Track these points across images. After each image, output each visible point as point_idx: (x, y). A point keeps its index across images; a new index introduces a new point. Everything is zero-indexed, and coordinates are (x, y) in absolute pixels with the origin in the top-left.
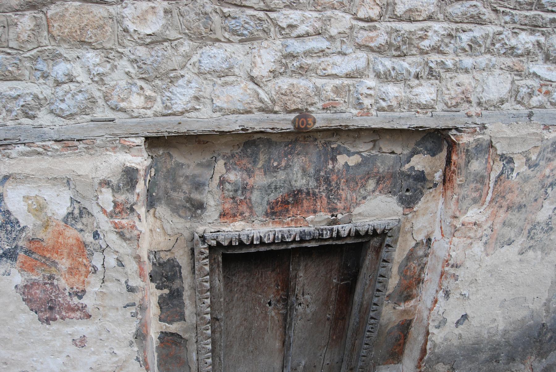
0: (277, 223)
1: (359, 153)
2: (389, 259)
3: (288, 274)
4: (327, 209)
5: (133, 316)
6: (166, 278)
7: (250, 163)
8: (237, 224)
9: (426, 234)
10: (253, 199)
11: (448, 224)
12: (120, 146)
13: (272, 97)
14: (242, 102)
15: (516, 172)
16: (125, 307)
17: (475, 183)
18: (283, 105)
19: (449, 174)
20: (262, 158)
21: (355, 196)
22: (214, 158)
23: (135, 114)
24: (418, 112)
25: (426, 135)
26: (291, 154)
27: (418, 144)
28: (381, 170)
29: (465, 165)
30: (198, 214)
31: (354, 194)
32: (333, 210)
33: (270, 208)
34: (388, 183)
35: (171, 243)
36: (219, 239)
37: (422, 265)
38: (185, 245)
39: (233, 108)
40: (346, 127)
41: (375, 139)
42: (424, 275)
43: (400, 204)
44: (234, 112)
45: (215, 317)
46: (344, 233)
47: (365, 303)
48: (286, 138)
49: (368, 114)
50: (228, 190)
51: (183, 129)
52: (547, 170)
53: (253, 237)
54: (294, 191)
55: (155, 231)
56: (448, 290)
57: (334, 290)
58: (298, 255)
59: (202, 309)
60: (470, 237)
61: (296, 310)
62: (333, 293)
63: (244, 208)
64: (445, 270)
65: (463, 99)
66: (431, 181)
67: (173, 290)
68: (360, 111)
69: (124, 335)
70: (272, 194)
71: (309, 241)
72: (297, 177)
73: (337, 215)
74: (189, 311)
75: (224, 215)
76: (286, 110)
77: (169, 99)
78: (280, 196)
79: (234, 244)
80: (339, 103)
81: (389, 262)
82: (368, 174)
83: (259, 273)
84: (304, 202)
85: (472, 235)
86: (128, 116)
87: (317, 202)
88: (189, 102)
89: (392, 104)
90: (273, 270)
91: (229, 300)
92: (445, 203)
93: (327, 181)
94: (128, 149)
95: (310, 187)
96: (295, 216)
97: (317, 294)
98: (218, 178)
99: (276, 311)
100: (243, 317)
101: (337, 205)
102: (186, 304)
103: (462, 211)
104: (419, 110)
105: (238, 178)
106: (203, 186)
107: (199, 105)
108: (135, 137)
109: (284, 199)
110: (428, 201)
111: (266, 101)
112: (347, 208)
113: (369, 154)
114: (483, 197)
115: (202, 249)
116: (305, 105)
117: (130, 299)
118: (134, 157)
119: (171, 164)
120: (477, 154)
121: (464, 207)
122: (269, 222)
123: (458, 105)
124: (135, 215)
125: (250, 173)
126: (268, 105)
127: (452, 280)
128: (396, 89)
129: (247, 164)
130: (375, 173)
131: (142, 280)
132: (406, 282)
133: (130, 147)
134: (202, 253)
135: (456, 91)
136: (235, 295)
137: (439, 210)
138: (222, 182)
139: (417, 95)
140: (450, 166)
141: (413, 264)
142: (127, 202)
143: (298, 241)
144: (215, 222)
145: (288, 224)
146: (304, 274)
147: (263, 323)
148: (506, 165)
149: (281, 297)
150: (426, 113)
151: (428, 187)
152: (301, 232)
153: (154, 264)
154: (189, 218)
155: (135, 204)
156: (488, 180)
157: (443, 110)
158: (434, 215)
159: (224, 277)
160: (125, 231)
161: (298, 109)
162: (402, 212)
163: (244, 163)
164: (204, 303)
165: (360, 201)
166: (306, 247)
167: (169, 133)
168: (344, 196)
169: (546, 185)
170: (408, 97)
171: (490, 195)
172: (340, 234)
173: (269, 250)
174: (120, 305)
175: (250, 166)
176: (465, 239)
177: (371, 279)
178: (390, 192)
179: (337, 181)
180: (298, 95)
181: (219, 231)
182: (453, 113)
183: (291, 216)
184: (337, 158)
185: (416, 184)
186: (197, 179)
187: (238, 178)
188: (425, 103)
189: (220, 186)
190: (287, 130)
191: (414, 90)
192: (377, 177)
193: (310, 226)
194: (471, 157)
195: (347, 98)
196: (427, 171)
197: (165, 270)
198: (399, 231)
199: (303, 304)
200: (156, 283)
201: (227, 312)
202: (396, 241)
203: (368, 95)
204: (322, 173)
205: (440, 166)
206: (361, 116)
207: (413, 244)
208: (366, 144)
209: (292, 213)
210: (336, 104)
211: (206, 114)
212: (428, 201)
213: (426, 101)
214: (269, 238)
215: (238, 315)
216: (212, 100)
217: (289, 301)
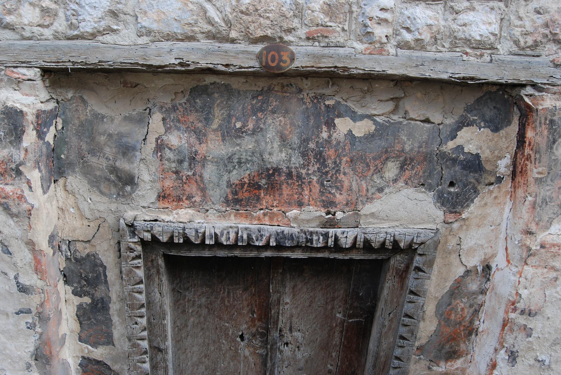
0: (242, 216)
1: (370, 117)
2: (419, 291)
3: (268, 296)
4: (320, 202)
5: (29, 328)
6: (86, 281)
7: (201, 121)
8: (182, 212)
9: (483, 257)
10: (206, 176)
11: (517, 243)
12: (6, 79)
13: (226, 15)
14: (180, 21)
16: (17, 313)
18: (243, 30)
19: (521, 161)
20: (218, 114)
21: (364, 186)
22: (148, 110)
23: (27, 34)
24: (467, 54)
25: (484, 96)
26: (262, 111)
27: (469, 109)
28: (407, 148)
29: (547, 146)
30: (126, 191)
31: (363, 182)
32: (329, 204)
33: (233, 193)
34: (419, 169)
35: (91, 232)
36: (155, 232)
37: (476, 306)
38: (111, 237)
39: (166, 30)
40: (345, 71)
41: (397, 95)
42: (478, 323)
43: (439, 204)
44: (169, 37)
45: (157, 346)
46: (346, 242)
47: (382, 354)
48: (253, 84)
49: (381, 50)
50: (169, 160)
51: (93, 59)
53: (204, 233)
54: (268, 170)
55: (68, 211)
56: (514, 350)
57: (338, 329)
58: (281, 271)
59: (135, 332)
60: (553, 268)
61: (281, 352)
62: (336, 334)
63: (192, 189)
64: (510, 317)
65: (547, 36)
66: (492, 173)
67: (96, 299)
68: (370, 46)
69: (19, 353)
70: (235, 172)
71: (292, 249)
72: (272, 148)
73: (335, 213)
74: (118, 332)
75: (164, 197)
76: (249, 38)
77: (75, 13)
78: (247, 175)
79: (176, 241)
80: (334, 31)
81: (419, 296)
82: (386, 152)
83: (224, 290)
84: (284, 187)
86: (18, 37)
87: (303, 190)
88: (102, 18)
89: (423, 37)
90: (245, 290)
91: (181, 324)
92: (513, 209)
93: (320, 158)
94: (17, 83)
95: (293, 166)
96: (270, 208)
97: (312, 331)
98: (154, 140)
99: (252, 349)
100: (202, 352)
101: (335, 196)
102: (114, 321)
103: (541, 223)
104: (468, 50)
105: (183, 142)
106: (133, 150)
107: (117, 25)
108: (26, 67)
109: (253, 181)
110: (486, 204)
111: (217, 23)
112: (352, 204)
113: (387, 119)
115: (131, 244)
116: (278, 30)
117: (23, 302)
118: (25, 97)
119: (85, 114)
121: (546, 218)
122: (230, 214)
123: (537, 46)
124: (23, 181)
125: (201, 136)
126: (220, 28)
127: (521, 336)
128: (429, 13)
129: (195, 122)
130: (398, 151)
131: (39, 277)
132: (449, 330)
133: (19, 82)
134: (131, 250)
135: (533, 21)
136: (189, 319)
137: (505, 220)
138: (160, 147)
139: (465, 25)
140: (524, 149)
141: (461, 304)
142: (10, 160)
143: (273, 247)
144: (151, 206)
145: (259, 219)
146: (291, 301)
147: (232, 364)
149: (257, 330)
150: (482, 55)
151: (487, 181)
152: (278, 234)
153: (67, 259)
154: (115, 196)
155: (21, 164)
157: (511, 53)
158: (497, 229)
159: (173, 290)
160: (11, 203)
161: (267, 36)
162: (443, 217)
163: (191, 120)
164: (136, 323)
165: (373, 194)
166: (288, 258)
167: (74, 63)
168: (346, 184)
170: (450, 28)
172: (339, 243)
173: (232, 257)
174: (11, 310)
175: (200, 125)
176: (545, 270)
177: (392, 319)
178: (422, 185)
179: (335, 159)
180: (268, 15)
181: (156, 220)
182: (527, 59)
183: (264, 207)
184: (335, 122)
185: (467, 176)
186: (124, 140)
187: (183, 142)
188: (478, 38)
189: (157, 153)
190: (250, 70)
191: (461, 16)
192: (401, 159)
193: (292, 225)
195: (347, 23)
196: (485, 154)
197: (84, 270)
198: (436, 248)
199: (291, 344)
200: (72, 286)
201: (179, 341)
202: (431, 264)
203: (381, 19)
204: (312, 145)
205: (507, 148)
206: (370, 54)
207: (461, 271)
208: (382, 104)
209: (265, 204)
210: (329, 32)
211: (127, 39)
212: (486, 204)
213: (481, 35)
214: (229, 238)
215: (195, 349)
216: (137, 17)
217: (270, 338)
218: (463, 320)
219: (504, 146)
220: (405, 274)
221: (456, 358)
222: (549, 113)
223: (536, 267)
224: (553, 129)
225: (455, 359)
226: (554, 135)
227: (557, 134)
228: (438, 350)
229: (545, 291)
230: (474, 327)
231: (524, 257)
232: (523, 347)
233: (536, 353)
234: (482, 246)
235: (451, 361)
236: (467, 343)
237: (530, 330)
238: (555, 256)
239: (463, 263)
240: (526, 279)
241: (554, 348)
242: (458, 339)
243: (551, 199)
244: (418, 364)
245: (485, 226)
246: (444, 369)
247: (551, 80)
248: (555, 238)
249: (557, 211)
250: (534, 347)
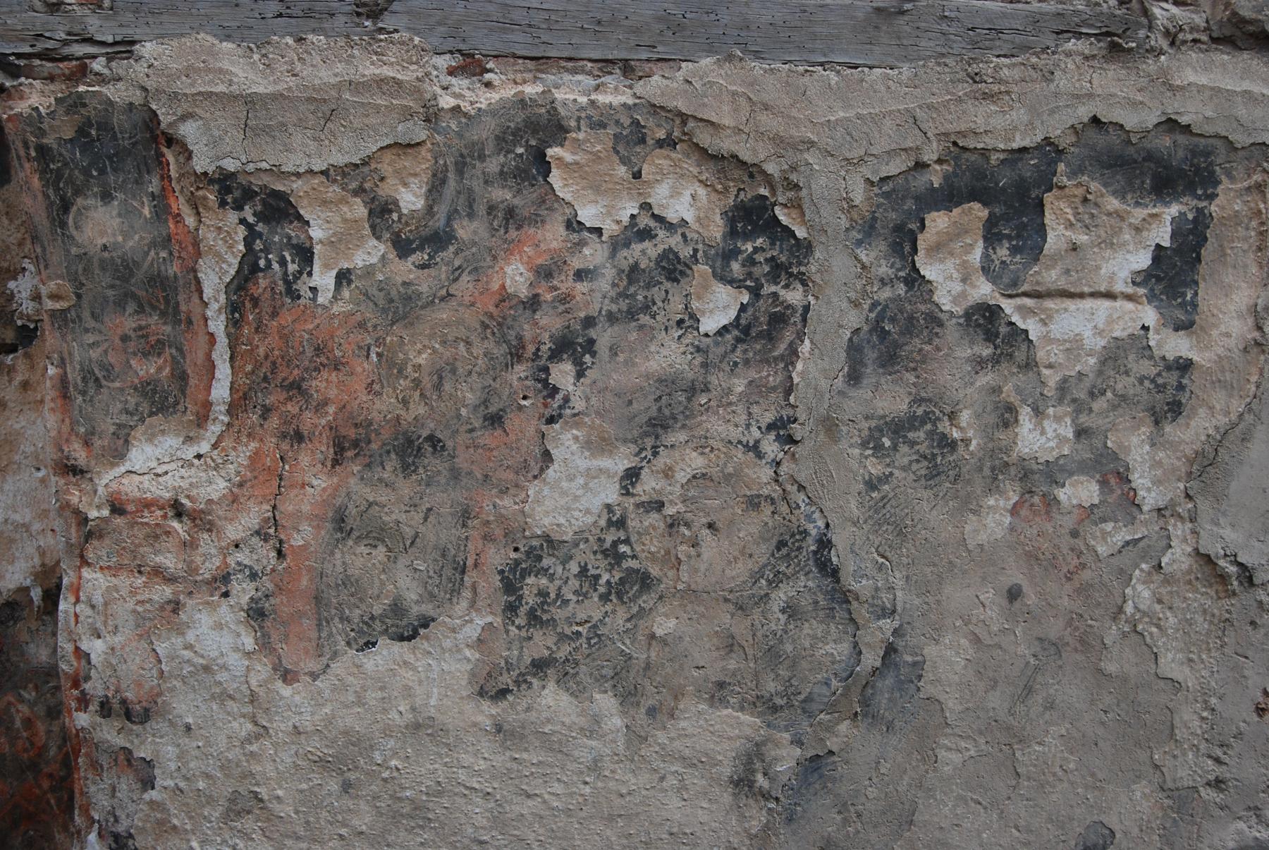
15: (327, 266)
17: (130, 310)
52: (509, 270)
56: (121, 829)
85: (169, 561)
103: (98, 443)
114: (192, 382)
120: (102, 172)
148: (260, 227)
156: (196, 299)
169: (531, 349)
171: (223, 371)
176: (140, 581)
194: (71, 181)
218: (39, 755)
219: (11, 239)
222: (29, 129)
223: (114, 570)
224: (51, 171)
226: (60, 189)
227: (66, 183)
229: (152, 643)
231: (73, 541)
232: (140, 819)
233: (188, 841)
234: (26, 527)
237: (145, 765)
238: (157, 537)
240: (93, 607)
241: (238, 825)
243: (107, 370)
245: (19, 468)
247: (41, 46)
248: (146, 485)
249: (137, 404)
250: (175, 821)
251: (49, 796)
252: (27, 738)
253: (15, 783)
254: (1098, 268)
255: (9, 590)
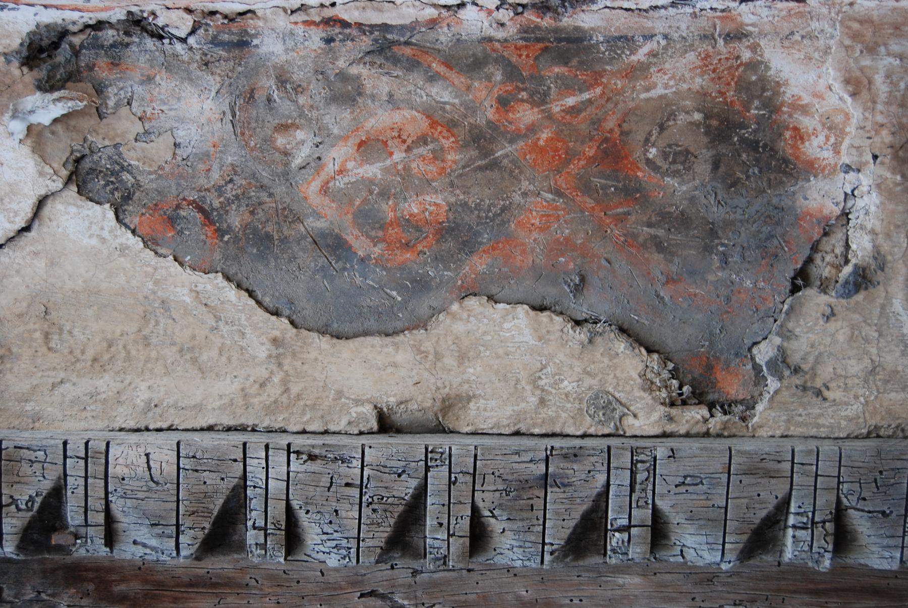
220: (124, 580)
221: (772, 105)
225: (777, 110)
228: (708, 249)
230: (512, 30)
235: (799, 135)
236: (641, 55)
239: (20, 223)
242: (611, 123)
244: (825, 372)
246: (865, 180)
251: (556, 109)
252: (409, 150)
253: (525, 185)
254: (784, 92)
255: (41, 174)
